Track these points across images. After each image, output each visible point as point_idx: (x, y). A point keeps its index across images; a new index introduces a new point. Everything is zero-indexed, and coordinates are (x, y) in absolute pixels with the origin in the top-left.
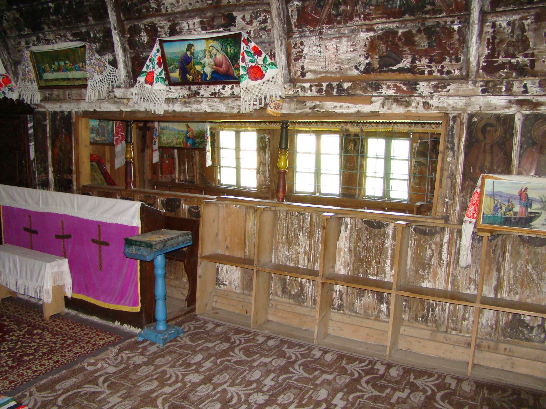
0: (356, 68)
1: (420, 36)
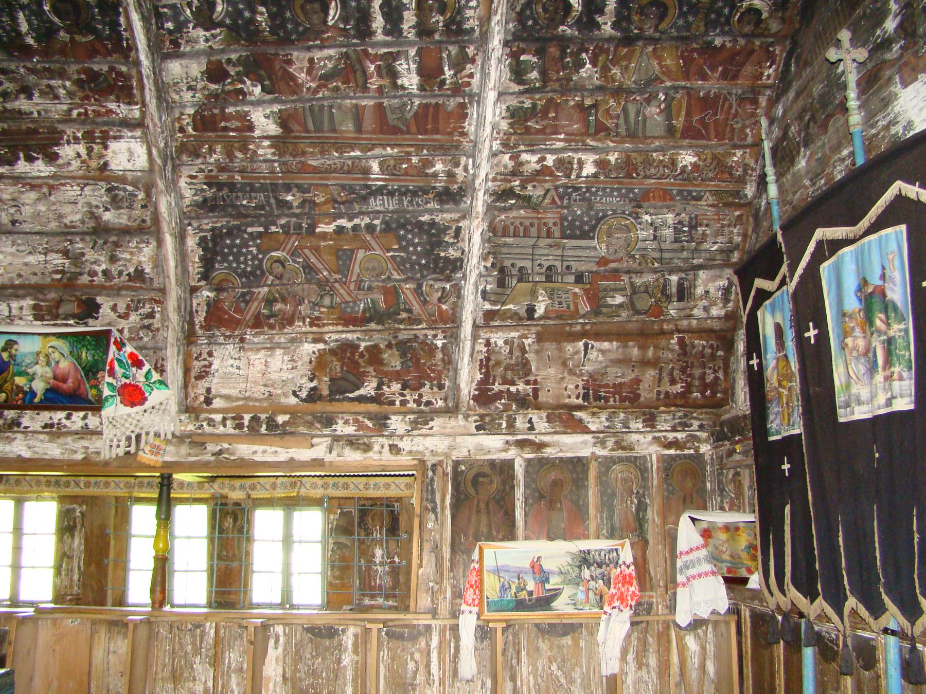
0: (295, 394)
1: (390, 352)
